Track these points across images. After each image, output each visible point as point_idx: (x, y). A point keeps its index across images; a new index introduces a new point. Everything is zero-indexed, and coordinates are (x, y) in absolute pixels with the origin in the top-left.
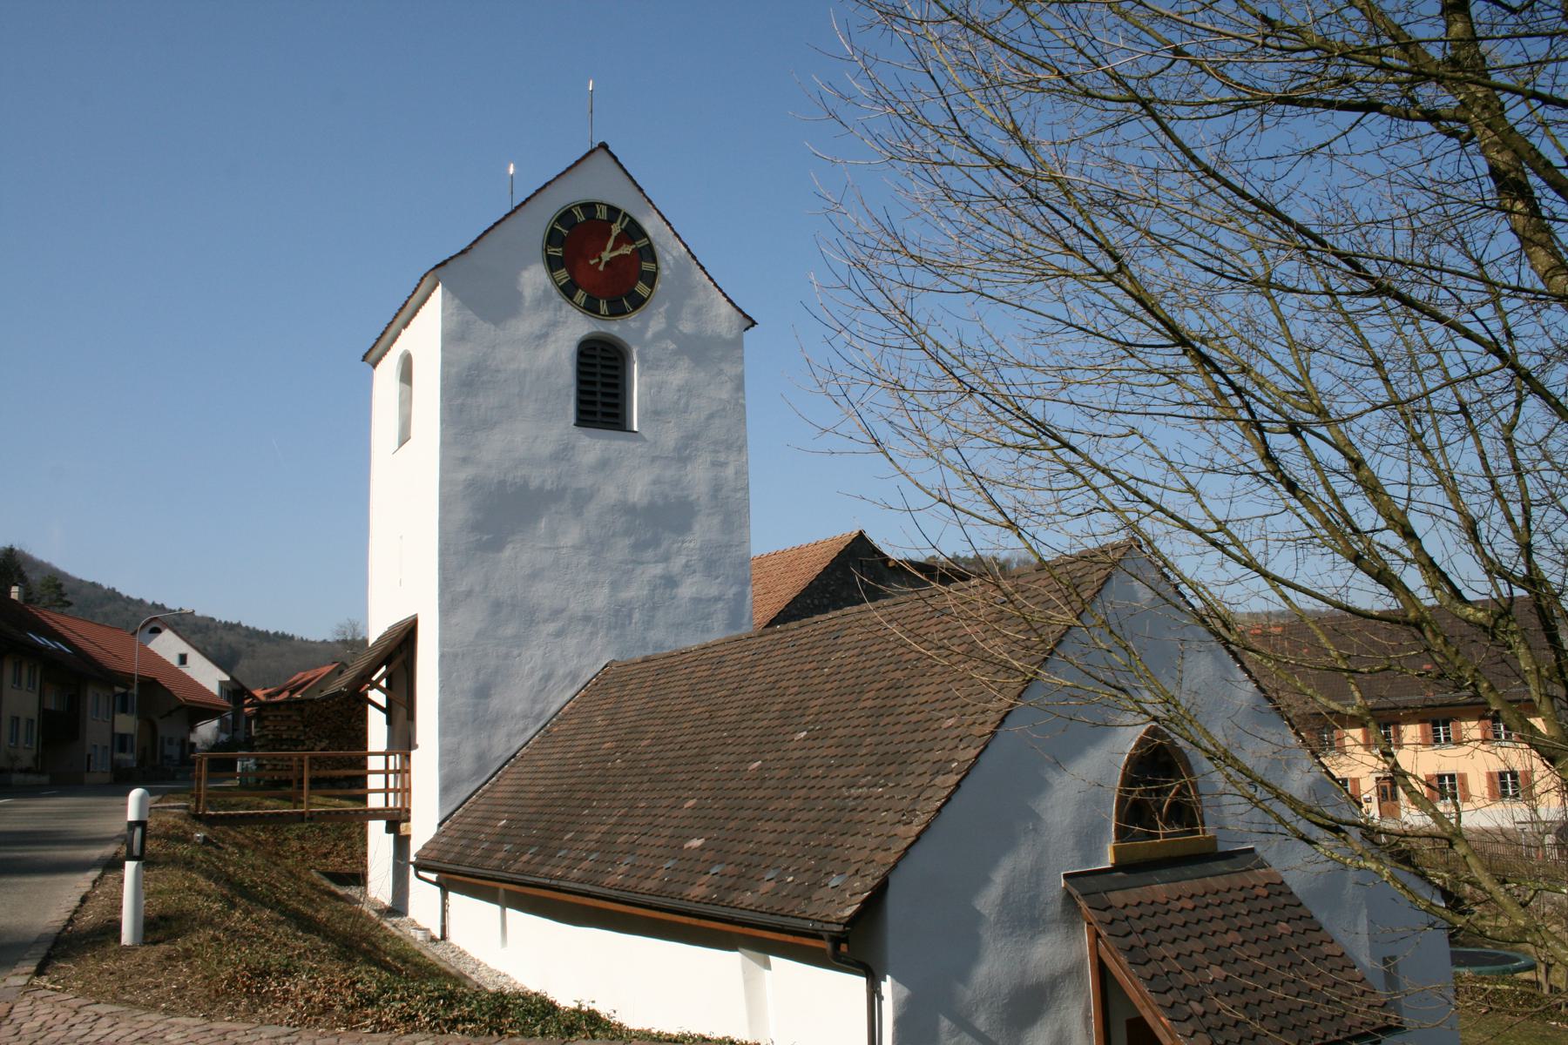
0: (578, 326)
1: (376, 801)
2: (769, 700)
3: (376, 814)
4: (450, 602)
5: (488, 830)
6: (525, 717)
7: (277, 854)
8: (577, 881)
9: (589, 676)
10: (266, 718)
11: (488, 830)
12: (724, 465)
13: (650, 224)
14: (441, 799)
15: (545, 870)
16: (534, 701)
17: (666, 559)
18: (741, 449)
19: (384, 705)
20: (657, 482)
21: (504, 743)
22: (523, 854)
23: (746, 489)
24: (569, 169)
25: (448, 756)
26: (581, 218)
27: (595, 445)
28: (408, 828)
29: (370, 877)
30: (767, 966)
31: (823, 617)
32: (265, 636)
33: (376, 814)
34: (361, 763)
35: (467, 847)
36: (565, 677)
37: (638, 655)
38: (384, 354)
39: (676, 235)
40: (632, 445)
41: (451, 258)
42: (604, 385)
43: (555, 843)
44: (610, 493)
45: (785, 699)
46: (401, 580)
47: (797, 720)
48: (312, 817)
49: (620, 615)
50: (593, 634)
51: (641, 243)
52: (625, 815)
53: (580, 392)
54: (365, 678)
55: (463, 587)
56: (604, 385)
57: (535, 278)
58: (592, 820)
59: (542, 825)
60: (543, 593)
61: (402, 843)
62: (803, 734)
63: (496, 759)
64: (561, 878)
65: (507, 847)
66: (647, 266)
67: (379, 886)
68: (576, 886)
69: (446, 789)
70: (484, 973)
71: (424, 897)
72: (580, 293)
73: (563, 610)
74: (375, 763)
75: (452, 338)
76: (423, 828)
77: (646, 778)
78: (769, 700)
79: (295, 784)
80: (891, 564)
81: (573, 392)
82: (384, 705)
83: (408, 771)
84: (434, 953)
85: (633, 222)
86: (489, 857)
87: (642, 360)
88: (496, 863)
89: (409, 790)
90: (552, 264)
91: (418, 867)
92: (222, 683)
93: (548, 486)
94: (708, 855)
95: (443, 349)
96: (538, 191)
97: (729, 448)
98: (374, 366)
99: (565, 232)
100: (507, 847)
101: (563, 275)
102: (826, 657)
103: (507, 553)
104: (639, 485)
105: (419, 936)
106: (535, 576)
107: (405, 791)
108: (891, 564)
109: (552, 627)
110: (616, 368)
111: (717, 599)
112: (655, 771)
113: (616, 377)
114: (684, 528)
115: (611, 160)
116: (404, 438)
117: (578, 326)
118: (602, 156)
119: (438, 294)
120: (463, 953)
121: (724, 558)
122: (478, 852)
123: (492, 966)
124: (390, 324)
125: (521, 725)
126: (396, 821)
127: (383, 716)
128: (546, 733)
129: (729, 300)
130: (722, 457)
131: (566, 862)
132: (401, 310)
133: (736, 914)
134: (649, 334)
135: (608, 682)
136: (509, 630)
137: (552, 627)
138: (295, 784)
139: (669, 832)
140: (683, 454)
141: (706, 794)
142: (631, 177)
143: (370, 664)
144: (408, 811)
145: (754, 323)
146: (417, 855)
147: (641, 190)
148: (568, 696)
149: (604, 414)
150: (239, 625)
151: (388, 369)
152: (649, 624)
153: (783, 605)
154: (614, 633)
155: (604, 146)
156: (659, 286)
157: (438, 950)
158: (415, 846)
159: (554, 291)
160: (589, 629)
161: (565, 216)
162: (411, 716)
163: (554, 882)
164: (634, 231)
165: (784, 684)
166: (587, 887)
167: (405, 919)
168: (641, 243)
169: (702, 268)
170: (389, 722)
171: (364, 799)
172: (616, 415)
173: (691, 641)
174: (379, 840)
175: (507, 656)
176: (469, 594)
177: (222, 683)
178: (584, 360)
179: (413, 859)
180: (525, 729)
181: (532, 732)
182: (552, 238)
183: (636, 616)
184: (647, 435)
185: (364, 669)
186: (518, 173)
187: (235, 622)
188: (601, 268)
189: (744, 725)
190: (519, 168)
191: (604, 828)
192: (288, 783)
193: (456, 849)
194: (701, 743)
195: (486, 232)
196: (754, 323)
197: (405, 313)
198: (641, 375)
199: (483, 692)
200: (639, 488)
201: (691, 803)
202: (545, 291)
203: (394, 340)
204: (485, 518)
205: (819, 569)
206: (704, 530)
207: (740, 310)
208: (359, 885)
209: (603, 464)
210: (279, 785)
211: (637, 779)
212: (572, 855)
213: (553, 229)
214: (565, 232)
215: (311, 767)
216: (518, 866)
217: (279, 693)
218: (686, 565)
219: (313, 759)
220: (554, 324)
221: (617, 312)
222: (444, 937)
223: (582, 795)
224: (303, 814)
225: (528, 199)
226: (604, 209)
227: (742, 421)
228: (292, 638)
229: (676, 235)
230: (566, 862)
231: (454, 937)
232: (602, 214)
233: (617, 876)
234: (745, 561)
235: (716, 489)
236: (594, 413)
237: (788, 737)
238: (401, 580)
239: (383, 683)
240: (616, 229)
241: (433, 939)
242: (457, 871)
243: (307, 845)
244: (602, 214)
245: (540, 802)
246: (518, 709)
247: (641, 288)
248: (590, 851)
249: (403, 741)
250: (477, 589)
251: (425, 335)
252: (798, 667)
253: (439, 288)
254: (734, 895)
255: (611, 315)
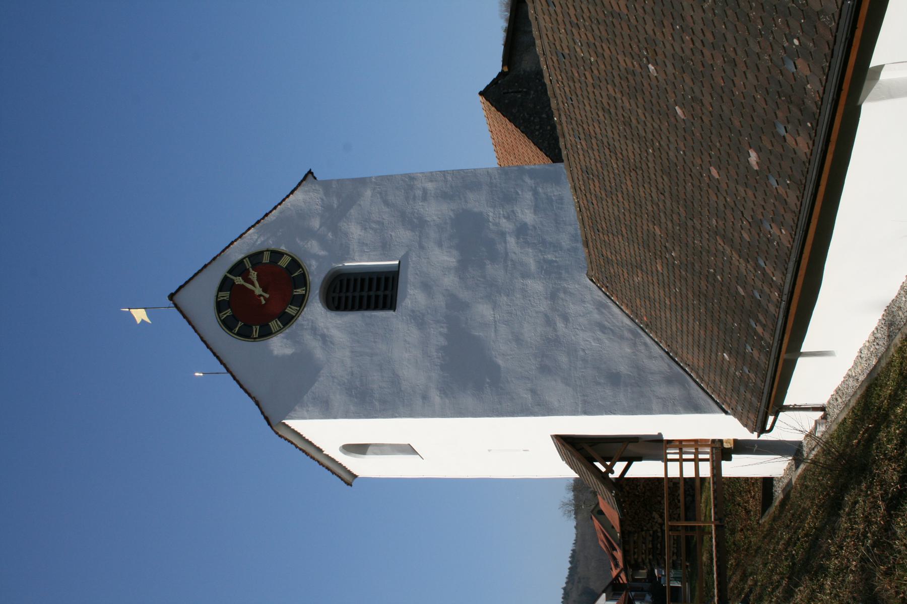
0: (315, 311)
1: (705, 470)
2: (620, 111)
3: (716, 469)
4: (540, 407)
5: (732, 369)
6: (635, 344)
7: (747, 550)
8: (785, 275)
9: (601, 293)
10: (636, 561)
11: (732, 369)
12: (425, 191)
13: (236, 254)
14: (705, 412)
15: (772, 309)
16: (622, 338)
17: (503, 234)
18: (412, 178)
19: (625, 464)
20: (440, 245)
21: (656, 361)
22: (756, 333)
23: (444, 173)
24: (190, 323)
25: (669, 407)
26: (229, 312)
27: (411, 296)
28: (728, 441)
29: (767, 475)
30: (880, 68)
31: (546, 75)
32: (573, 571)
33: (716, 469)
34: (674, 483)
35: (747, 386)
36: (601, 313)
37: (582, 252)
38: (345, 468)
39: (241, 237)
40: (411, 271)
41: (262, 413)
42: (362, 289)
43: (747, 303)
44: (450, 281)
45: (619, 96)
46: (520, 449)
47: (638, 79)
48: (719, 518)
49: (550, 270)
50: (565, 291)
51: (248, 264)
52: (724, 237)
53: (368, 308)
54: (603, 477)
55: (528, 397)
56: (362, 289)
57: (279, 345)
58: (727, 270)
59: (729, 319)
60: (532, 332)
61: (741, 447)
62: (651, 67)
63: (671, 368)
64: (781, 296)
65: (749, 349)
66: (266, 259)
67: (774, 467)
68: (789, 276)
69: (696, 409)
70: (858, 370)
71: (788, 427)
72: (288, 310)
73: (546, 316)
74: (674, 471)
75: (327, 411)
76: (727, 427)
77: (690, 223)
78: (620, 111)
79: (690, 534)
80: (506, 69)
81: (367, 313)
82: (625, 464)
83: (681, 441)
84: (837, 414)
85: (231, 271)
86: (758, 365)
87: (346, 260)
88: (762, 357)
89: (696, 441)
90: (266, 333)
91: (763, 430)
92: (608, 599)
93: (445, 330)
94: (766, 143)
95: (335, 418)
96: (208, 347)
97: (411, 187)
98: (355, 476)
99: (240, 324)
100: (749, 349)
101: (274, 324)
102: (580, 63)
103: (500, 362)
104: (441, 259)
105: (822, 428)
106: (518, 340)
107: (697, 444)
108: (506, 69)
109: (560, 325)
110: (348, 280)
111: (535, 193)
112: (683, 214)
113: (356, 280)
114: (479, 220)
115: (183, 291)
116: (409, 450)
117: (315, 311)
118: (178, 298)
119: (292, 423)
120: (838, 391)
121: (502, 186)
122: (752, 376)
123: (851, 364)
124: (297, 447)
125: (642, 348)
126: (722, 451)
127: (635, 464)
128: (648, 327)
129: (292, 192)
130: (419, 193)
131: (766, 289)
132: (307, 454)
133: (830, 97)
134: (323, 253)
135: (605, 278)
136: (563, 359)
137: (560, 325)
138: (690, 534)
139: (741, 189)
140: (418, 224)
141: (706, 158)
142: (196, 275)
143: (593, 473)
144: (713, 441)
145: (310, 172)
146: (752, 432)
147: (205, 266)
148: (616, 310)
149: (386, 288)
150: (564, 589)
151: (356, 465)
152: (557, 247)
153: (541, 153)
154: (564, 275)
155: (171, 297)
156: (283, 248)
157: (834, 412)
158: (745, 434)
159: (287, 331)
160: (562, 295)
161: (228, 325)
162: (634, 439)
163: (785, 298)
164: (238, 268)
165: (605, 101)
166: (791, 266)
167: (805, 443)
168: (248, 264)
169: (267, 215)
170: (640, 459)
171: (703, 480)
172: (387, 279)
173: (571, 213)
174: (738, 467)
175: (584, 360)
176: (533, 392)
177: (608, 599)
178: (343, 306)
179: (754, 436)
180: (645, 344)
181: (648, 340)
182: (245, 334)
183: (550, 257)
184: (402, 253)
185: (597, 477)
186: (201, 370)
187: (562, 591)
188: (267, 296)
189: (642, 133)
190: (196, 369)
191: (735, 256)
192: (688, 540)
193: (748, 395)
194: (659, 173)
195: (241, 386)
196: (310, 172)
197: (310, 451)
198: (354, 260)
199: (615, 379)
200: (446, 258)
201: (714, 172)
202: (286, 338)
203: (333, 460)
204: (472, 382)
205: (511, 126)
206: (477, 202)
207: (300, 184)
208: (772, 485)
209: (427, 287)
210: (689, 548)
211: (690, 233)
212: (759, 283)
213: (238, 334)
214: (240, 324)
215: (678, 519)
216: (767, 336)
217: (614, 559)
218: (508, 218)
219: (671, 518)
220: (314, 330)
221: (303, 281)
222: (822, 409)
223: (703, 283)
224: (716, 526)
225: (215, 354)
226: (221, 294)
227: (389, 178)
228: (573, 550)
229: (241, 237)
230: (766, 289)
231: (823, 400)
232: (225, 295)
233: (782, 235)
234: (503, 171)
235: (444, 196)
236: (385, 297)
237: (654, 82)
238: (520, 449)
239: (608, 463)
240: (239, 281)
241: (824, 418)
242: (764, 397)
243: (739, 527)
244: (225, 295)
245: (709, 323)
246: (628, 350)
247: (284, 262)
248: (757, 266)
249: (654, 447)
250: (529, 385)
251: (327, 433)
252: (590, 89)
253: (288, 422)
254: (809, 103)
255: (305, 285)
